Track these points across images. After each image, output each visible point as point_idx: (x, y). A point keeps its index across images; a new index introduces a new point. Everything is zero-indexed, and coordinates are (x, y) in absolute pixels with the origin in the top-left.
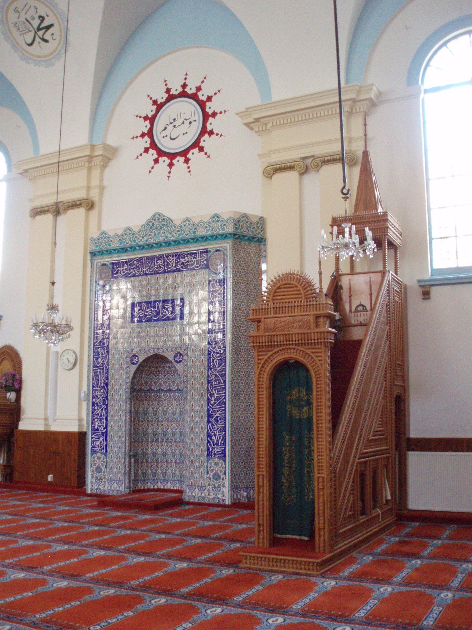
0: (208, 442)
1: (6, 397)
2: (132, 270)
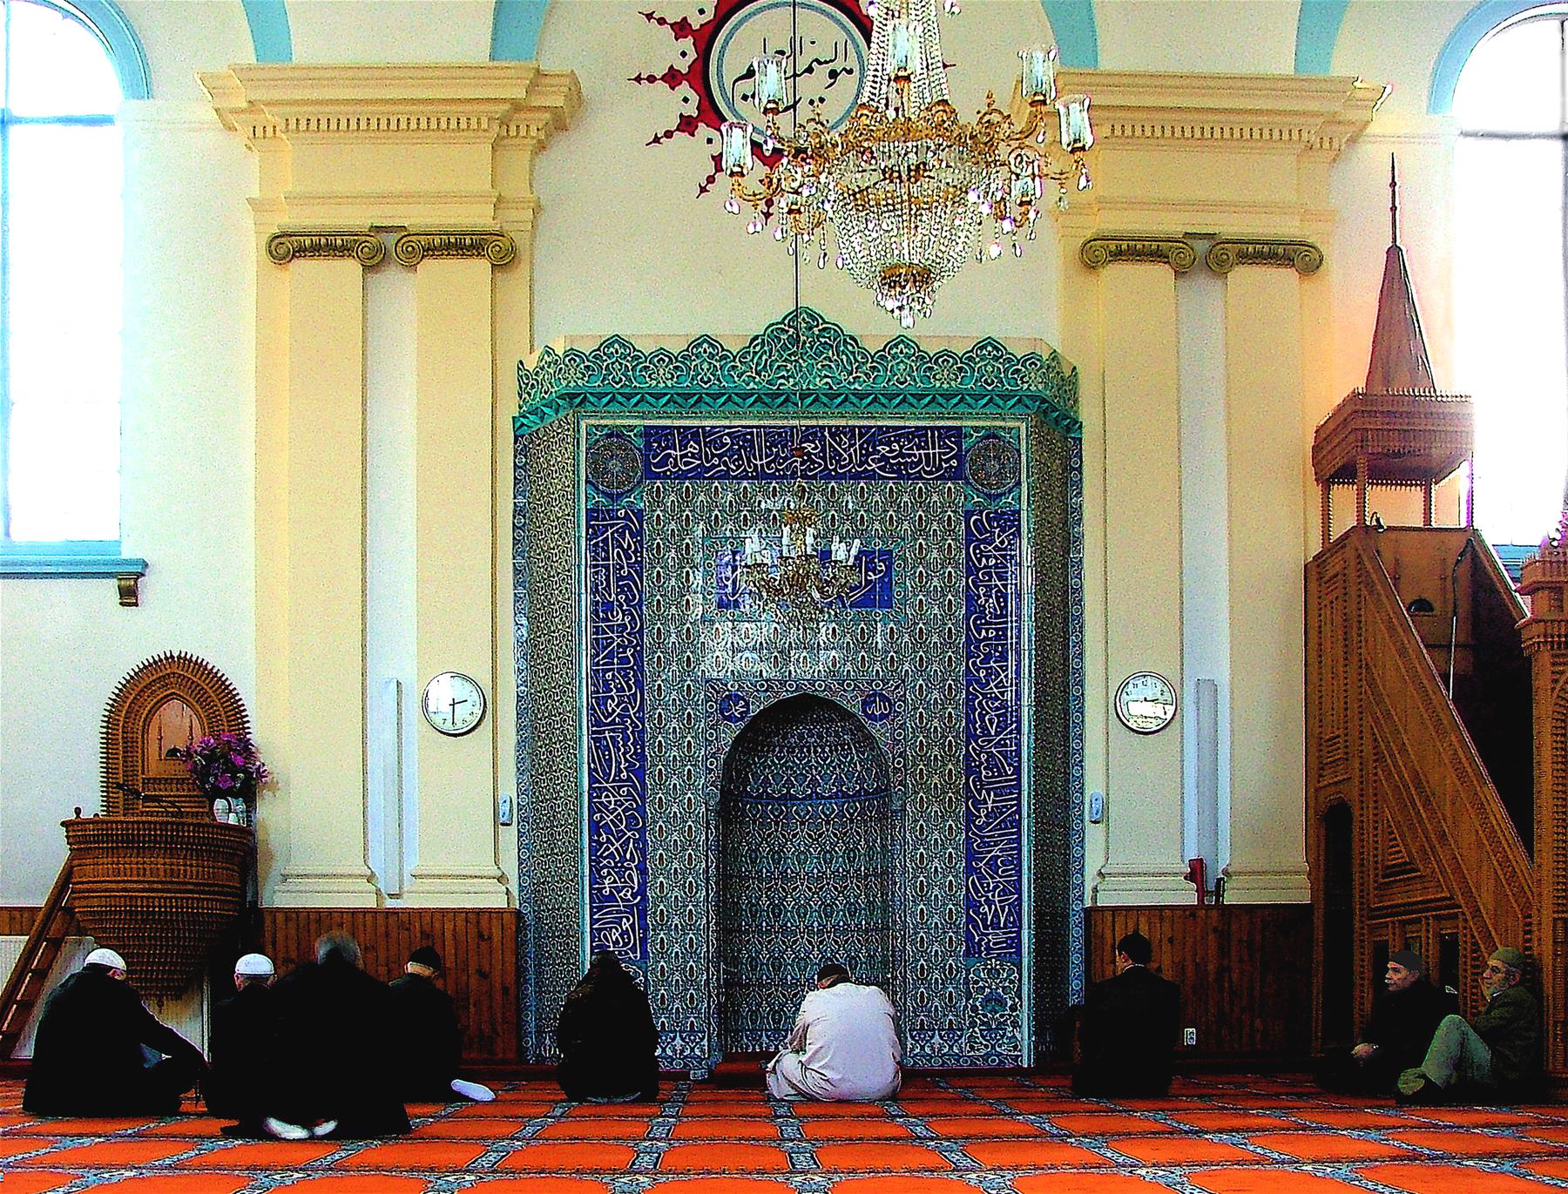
0: (970, 920)
1: (211, 813)
2: (716, 461)
